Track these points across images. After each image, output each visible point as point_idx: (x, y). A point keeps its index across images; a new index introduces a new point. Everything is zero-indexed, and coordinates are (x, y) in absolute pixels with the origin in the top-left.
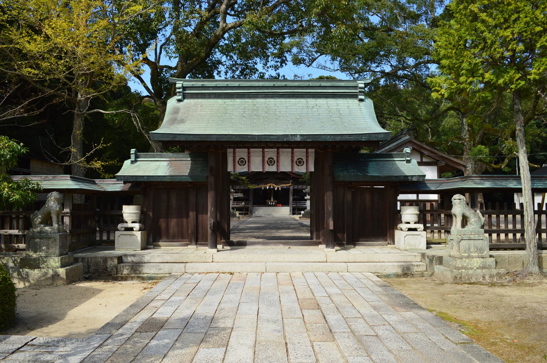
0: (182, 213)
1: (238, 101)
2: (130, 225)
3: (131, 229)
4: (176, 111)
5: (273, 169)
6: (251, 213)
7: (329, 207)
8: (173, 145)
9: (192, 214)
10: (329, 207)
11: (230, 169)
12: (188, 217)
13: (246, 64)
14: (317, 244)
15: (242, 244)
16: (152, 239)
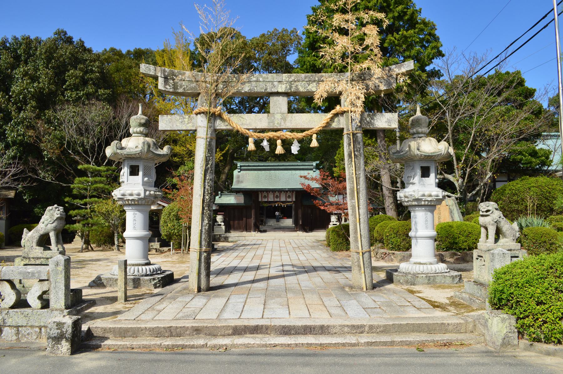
0: (240, 219)
1: (263, 172)
2: (220, 223)
3: (220, 225)
4: (238, 177)
5: (278, 200)
6: (265, 223)
7: (300, 216)
8: (237, 191)
9: (244, 219)
10: (300, 216)
11: (260, 200)
12: (242, 220)
13: (260, 60)
14: (296, 231)
15: (265, 231)
16: (228, 230)
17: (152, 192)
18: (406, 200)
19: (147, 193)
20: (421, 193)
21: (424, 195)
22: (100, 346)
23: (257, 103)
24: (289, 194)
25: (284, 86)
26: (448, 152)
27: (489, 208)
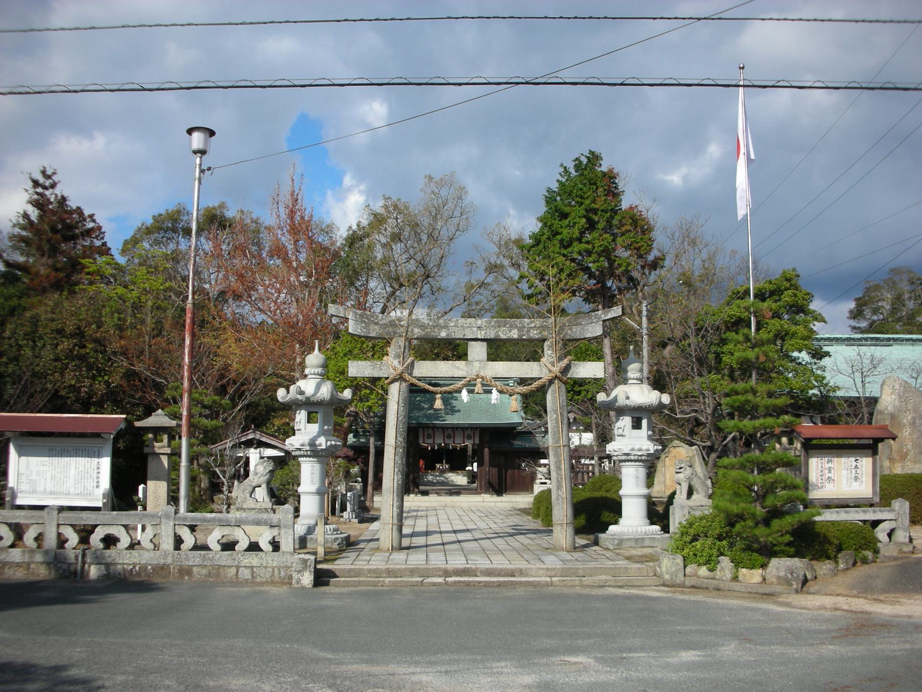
14: (480, 493)
17: (333, 443)
18: (616, 454)
19: (329, 443)
20: (630, 447)
21: (633, 449)
22: (329, 582)
23: (454, 350)
24: (469, 432)
25: (483, 332)
26: (660, 402)
27: (682, 465)
